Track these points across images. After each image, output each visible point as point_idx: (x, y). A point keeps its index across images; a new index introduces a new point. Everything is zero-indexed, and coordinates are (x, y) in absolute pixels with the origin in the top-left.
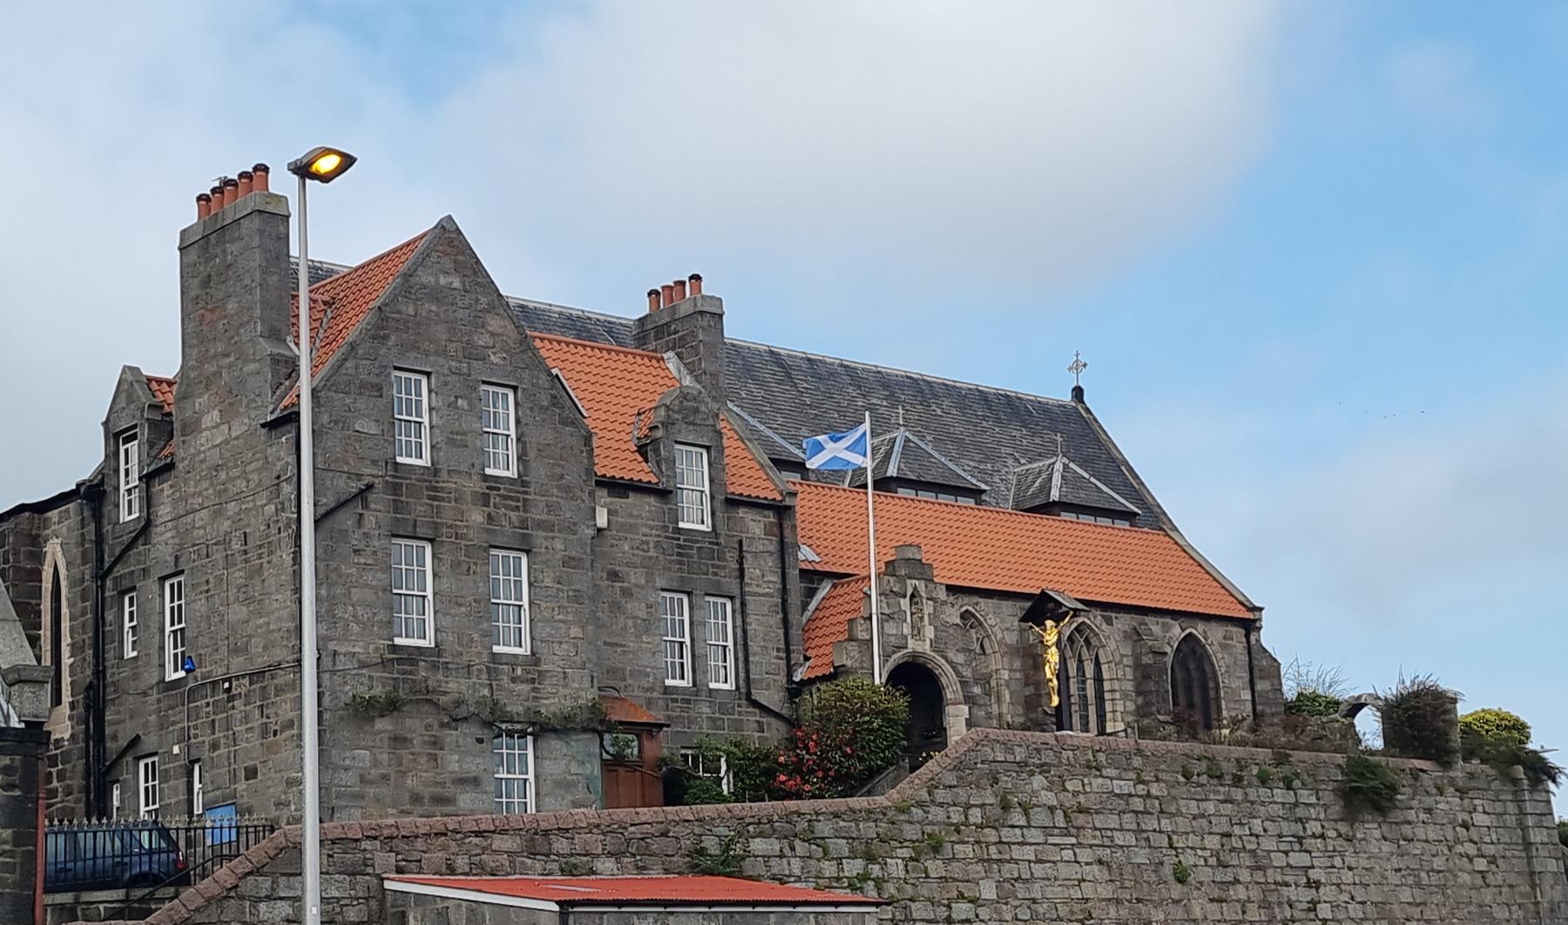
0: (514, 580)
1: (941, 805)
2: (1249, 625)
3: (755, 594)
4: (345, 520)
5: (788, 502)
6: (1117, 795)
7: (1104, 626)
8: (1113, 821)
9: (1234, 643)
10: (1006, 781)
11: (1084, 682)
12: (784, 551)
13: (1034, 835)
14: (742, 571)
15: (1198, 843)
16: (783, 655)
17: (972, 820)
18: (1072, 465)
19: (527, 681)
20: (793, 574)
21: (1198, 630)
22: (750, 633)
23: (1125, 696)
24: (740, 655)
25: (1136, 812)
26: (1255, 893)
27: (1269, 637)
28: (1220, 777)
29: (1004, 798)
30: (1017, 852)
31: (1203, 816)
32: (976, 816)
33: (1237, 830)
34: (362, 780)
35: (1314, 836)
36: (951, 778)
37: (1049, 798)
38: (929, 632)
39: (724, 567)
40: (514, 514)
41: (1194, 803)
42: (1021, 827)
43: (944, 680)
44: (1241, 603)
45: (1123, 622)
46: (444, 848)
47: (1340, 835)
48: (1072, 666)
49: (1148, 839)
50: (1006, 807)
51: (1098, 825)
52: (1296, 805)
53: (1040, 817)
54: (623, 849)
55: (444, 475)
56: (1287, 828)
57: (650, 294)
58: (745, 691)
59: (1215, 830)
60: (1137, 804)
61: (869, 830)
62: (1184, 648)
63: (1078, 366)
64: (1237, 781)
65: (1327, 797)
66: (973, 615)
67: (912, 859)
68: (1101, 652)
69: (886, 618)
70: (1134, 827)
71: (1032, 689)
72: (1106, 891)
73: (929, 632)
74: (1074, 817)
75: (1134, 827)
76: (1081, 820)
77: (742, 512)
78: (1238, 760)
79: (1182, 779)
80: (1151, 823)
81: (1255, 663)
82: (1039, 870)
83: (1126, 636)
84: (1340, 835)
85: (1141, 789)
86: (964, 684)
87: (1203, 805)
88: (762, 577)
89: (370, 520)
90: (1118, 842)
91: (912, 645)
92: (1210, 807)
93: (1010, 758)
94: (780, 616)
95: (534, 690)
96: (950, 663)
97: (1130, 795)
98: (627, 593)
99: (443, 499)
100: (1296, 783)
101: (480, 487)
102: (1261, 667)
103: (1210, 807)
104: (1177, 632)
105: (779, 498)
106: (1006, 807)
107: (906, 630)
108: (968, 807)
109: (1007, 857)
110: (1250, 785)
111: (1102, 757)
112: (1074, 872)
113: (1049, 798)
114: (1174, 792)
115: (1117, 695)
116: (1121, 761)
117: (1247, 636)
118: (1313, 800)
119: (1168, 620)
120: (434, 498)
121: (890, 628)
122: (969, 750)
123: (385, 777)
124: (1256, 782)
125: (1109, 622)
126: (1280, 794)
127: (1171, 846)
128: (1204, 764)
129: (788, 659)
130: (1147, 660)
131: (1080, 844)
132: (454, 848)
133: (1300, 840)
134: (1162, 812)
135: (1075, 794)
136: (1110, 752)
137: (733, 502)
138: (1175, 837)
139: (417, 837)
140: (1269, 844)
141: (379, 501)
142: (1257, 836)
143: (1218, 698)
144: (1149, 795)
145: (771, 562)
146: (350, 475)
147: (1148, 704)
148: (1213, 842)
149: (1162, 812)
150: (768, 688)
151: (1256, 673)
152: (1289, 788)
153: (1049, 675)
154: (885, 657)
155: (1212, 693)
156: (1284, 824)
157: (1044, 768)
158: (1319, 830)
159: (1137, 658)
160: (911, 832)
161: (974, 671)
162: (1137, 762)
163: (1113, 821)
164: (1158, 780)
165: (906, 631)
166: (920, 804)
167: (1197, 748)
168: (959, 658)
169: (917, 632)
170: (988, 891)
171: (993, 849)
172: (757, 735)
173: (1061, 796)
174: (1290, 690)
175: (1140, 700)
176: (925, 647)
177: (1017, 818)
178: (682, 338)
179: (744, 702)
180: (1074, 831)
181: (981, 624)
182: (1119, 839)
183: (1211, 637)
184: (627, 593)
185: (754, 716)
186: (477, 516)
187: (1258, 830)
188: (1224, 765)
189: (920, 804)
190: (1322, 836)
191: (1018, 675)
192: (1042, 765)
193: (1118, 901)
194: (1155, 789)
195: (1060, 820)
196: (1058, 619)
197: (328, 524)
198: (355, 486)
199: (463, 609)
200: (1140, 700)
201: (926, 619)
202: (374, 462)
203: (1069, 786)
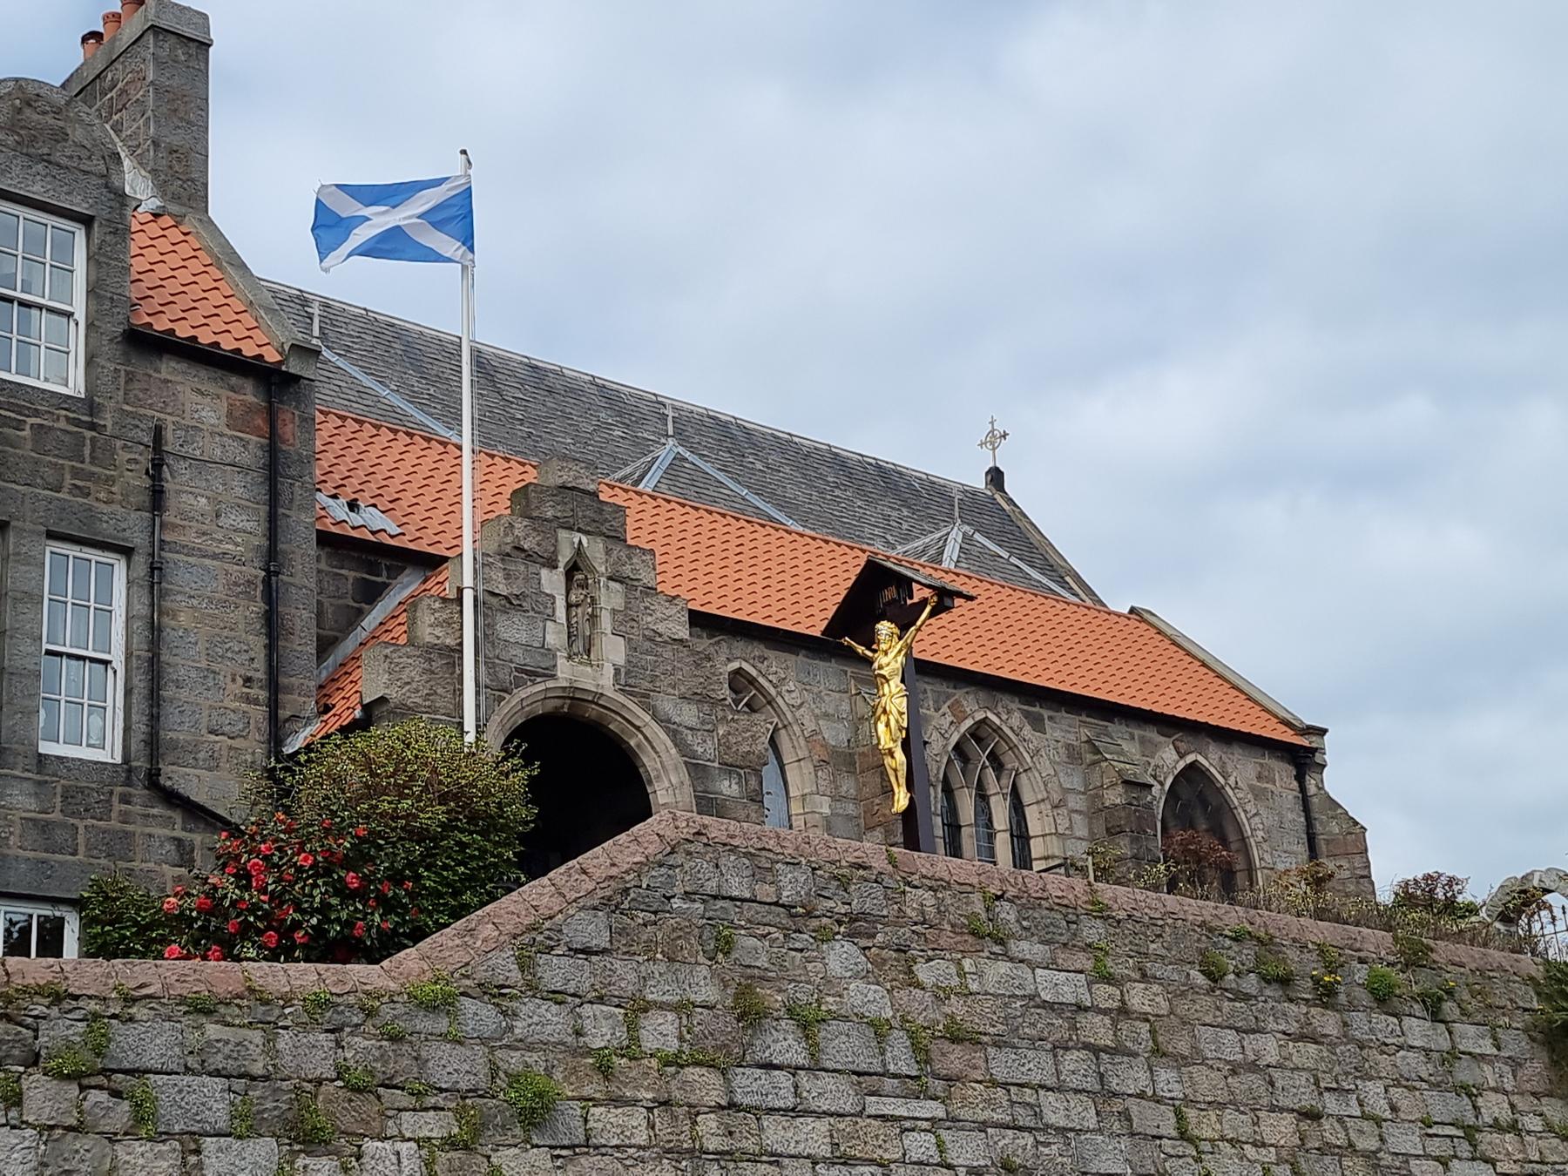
1: (556, 997)
2: (1301, 755)
3: (190, 551)
5: (294, 367)
6: (1045, 1005)
7: (1027, 731)
8: (1037, 1067)
9: (1277, 789)
10: (752, 949)
11: (991, 837)
12: (278, 474)
13: (830, 1092)
15: (1245, 1131)
16: (263, 695)
17: (649, 1042)
18: (977, 536)
21: (1210, 758)
22: (169, 635)
24: (140, 683)
25: (1096, 1050)
27: (1340, 780)
28: (1285, 981)
29: (743, 992)
31: (1253, 1067)
32: (660, 1032)
33: (1331, 1104)
35: (1496, 1126)
36: (594, 931)
37: (871, 998)
38: (613, 651)
39: (110, 480)
41: (1231, 1035)
43: (649, 762)
45: (1064, 730)
47: (1549, 1128)
49: (1126, 1116)
50: (751, 1015)
51: (1000, 1074)
52: (1453, 1055)
53: (844, 1046)
56: (1444, 1106)
57: (84, 39)
58: (148, 773)
59: (1285, 1102)
60: (1098, 1030)
61: (310, 1054)
62: (1185, 792)
63: (995, 438)
64: (1326, 995)
65: (1516, 1044)
66: (752, 681)
67: (450, 1143)
68: (1024, 781)
69: (492, 605)
70: (1091, 1083)
73: (613, 651)
74: (935, 1055)
75: (1091, 1083)
76: (954, 1059)
77: (169, 368)
78: (1321, 950)
79: (1200, 980)
80: (1131, 1077)
81: (1319, 828)
83: (1073, 755)
84: (1549, 1128)
85: (1105, 995)
86: (697, 770)
88: (216, 512)
90: (1052, 1118)
91: (566, 671)
93: (766, 892)
94: (259, 606)
96: (664, 722)
97: (1080, 1008)
100: (1449, 1007)
102: (1330, 839)
103: (1269, 1048)
104: (1170, 758)
105: (272, 356)
106: (751, 1015)
107: (555, 636)
108: (638, 1008)
109: (750, 1145)
110: (1352, 1007)
111: (1007, 913)
113: (871, 998)
114: (1182, 1007)
116: (1059, 928)
117: (1300, 778)
118: (1487, 1047)
119: (1151, 734)
121: (512, 629)
122: (647, 863)
124: (1364, 997)
125: (1037, 723)
126: (1418, 1030)
127: (1184, 1136)
128: (1248, 953)
129: (273, 705)
130: (1115, 796)
131: (953, 1120)
133: (1470, 1133)
134: (1157, 1051)
135: (941, 995)
136: (1027, 904)
137: (146, 344)
138: (1191, 1114)
140: (1405, 1140)
142: (1378, 1121)
144: (1124, 1011)
145: (242, 489)
148: (1281, 1129)
149: (1157, 1051)
150: (213, 764)
151: (1322, 847)
152: (1436, 1016)
154: (494, 691)
156: (1432, 1097)
157: (857, 926)
158: (1505, 1115)
159: (1094, 795)
160: (453, 1066)
161: (724, 745)
162: (1093, 931)
163: (1037, 1067)
164: (1144, 977)
165: (551, 640)
166: (493, 992)
167: (1232, 916)
168: (688, 715)
169: (582, 645)
171: (709, 1123)
172: (170, 872)
173: (902, 995)
174: (1389, 870)
177: (785, 1044)
178: (123, 91)
179: (139, 792)
180: (938, 1086)
182: (1055, 1110)
183: (1237, 775)
185: (166, 827)
187: (1380, 1107)
188: (1292, 954)
189: (493, 992)
190: (1514, 1127)
191: (851, 809)
194: (1138, 998)
195: (900, 1058)
196: (905, 621)
201: (606, 622)
203: (923, 972)
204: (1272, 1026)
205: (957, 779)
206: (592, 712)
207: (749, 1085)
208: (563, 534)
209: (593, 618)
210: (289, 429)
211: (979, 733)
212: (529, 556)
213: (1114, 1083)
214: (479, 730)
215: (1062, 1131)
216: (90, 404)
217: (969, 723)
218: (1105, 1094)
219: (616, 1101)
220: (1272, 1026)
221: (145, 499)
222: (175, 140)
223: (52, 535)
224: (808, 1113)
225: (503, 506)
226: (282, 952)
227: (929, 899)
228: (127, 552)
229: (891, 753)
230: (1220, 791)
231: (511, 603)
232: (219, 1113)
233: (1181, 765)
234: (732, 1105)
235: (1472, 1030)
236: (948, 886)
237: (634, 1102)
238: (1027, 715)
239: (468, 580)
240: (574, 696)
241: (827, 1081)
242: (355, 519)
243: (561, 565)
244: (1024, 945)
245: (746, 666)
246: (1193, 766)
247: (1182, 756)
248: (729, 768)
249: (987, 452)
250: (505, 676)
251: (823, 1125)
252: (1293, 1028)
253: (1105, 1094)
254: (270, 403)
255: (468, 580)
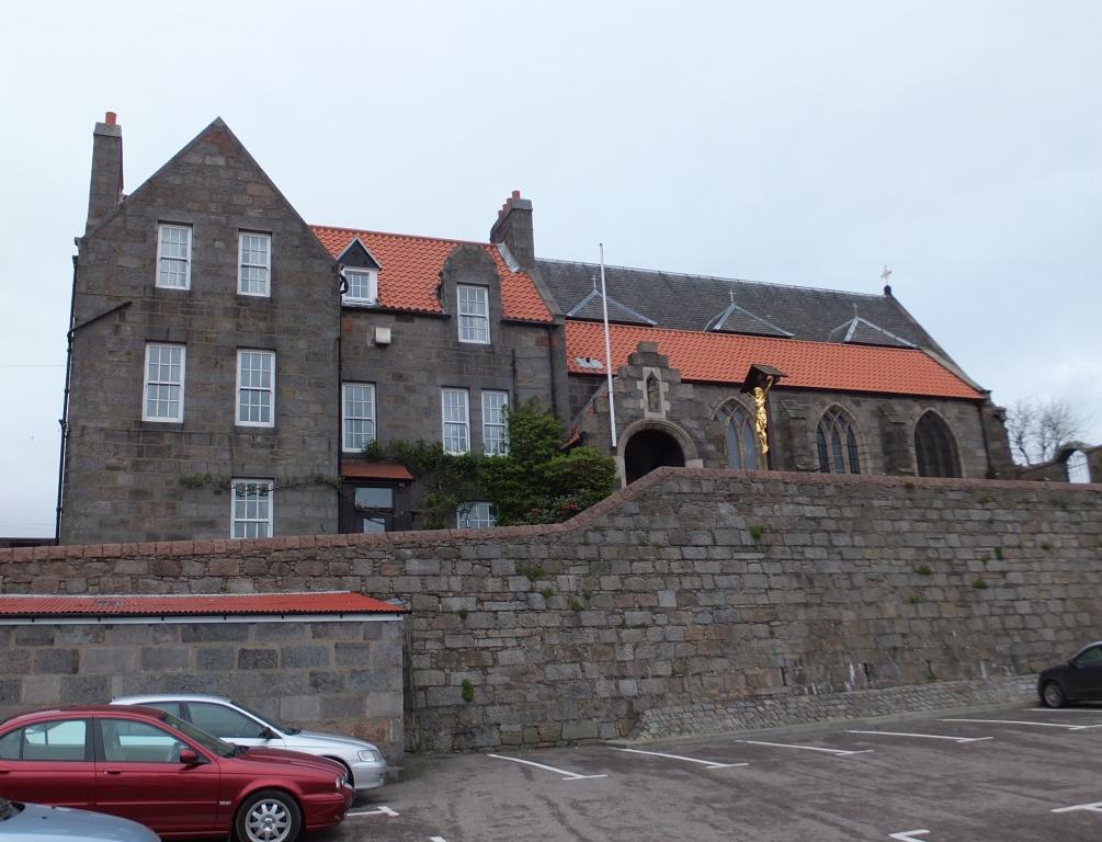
0: (255, 372)
4: (104, 330)
5: (557, 322)
6: (808, 518)
7: (854, 407)
8: (803, 539)
11: (840, 448)
12: (554, 356)
13: (718, 553)
14: (514, 371)
19: (267, 447)
20: (562, 376)
21: (936, 408)
23: (874, 457)
26: (954, 595)
30: (699, 567)
31: (898, 533)
33: (932, 543)
34: (102, 524)
38: (666, 406)
40: (260, 323)
42: (706, 546)
43: (681, 441)
44: (974, 389)
45: (870, 404)
46: (58, 571)
48: (829, 438)
49: (840, 553)
54: (263, 571)
55: (198, 295)
60: (830, 525)
63: (887, 274)
71: (789, 452)
72: (799, 597)
73: (666, 406)
75: (826, 543)
80: (841, 540)
82: (723, 582)
83: (873, 414)
85: (834, 513)
86: (698, 443)
87: (897, 524)
89: (127, 329)
90: (808, 556)
91: (648, 415)
92: (905, 525)
95: (272, 453)
98: (411, 390)
99: (195, 313)
101: (230, 303)
103: (905, 525)
104: (918, 410)
105: (550, 319)
107: (643, 403)
109: (689, 571)
112: (761, 582)
115: (868, 456)
119: (910, 402)
120: (188, 313)
121: (628, 404)
123: (124, 522)
125: (858, 404)
130: (889, 429)
132: (71, 570)
137: (508, 323)
139: (30, 562)
141: (135, 317)
143: (957, 457)
145: (543, 365)
146: (110, 298)
147: (892, 460)
153: (759, 429)
154: (621, 426)
155: (953, 453)
159: (882, 428)
163: (803, 539)
168: (694, 424)
169: (655, 407)
170: (668, 600)
171: (674, 565)
175: (887, 459)
176: (660, 417)
181: (745, 409)
183: (949, 414)
184: (411, 390)
186: (227, 325)
190: (1020, 547)
192: (730, 495)
193: (807, 605)
195: (747, 539)
197: (87, 332)
198: (113, 305)
199: (209, 394)
200: (887, 459)
201: (662, 396)
202: (134, 288)
204: (907, 517)
205: (824, 427)
206: (658, 428)
207: (689, 552)
208: (645, 369)
209: (658, 396)
210: (556, 342)
211: (833, 410)
212: (632, 378)
213: (836, 543)
214: (618, 439)
215: (812, 560)
216: (492, 346)
217: (828, 407)
218: (831, 547)
219: (641, 560)
220: (907, 517)
221: (511, 373)
222: (523, 246)
223: (483, 389)
224: (711, 560)
225: (625, 363)
226: (43, 644)
227: (761, 486)
228: (507, 391)
229: (761, 433)
230: (942, 420)
231: (627, 395)
232: (513, 569)
233: (924, 412)
234: (683, 559)
235: (1002, 512)
236: (769, 481)
237: (648, 560)
238: (853, 401)
239: (611, 390)
240: (651, 423)
241: (719, 550)
242: (588, 365)
243: (645, 379)
244: (800, 498)
245: (735, 398)
246: (930, 412)
247: (924, 408)
248: (710, 441)
249: (884, 279)
250: (626, 420)
251: (717, 563)
252: (917, 518)
253: (831, 547)
254: (550, 335)
255: (611, 390)
